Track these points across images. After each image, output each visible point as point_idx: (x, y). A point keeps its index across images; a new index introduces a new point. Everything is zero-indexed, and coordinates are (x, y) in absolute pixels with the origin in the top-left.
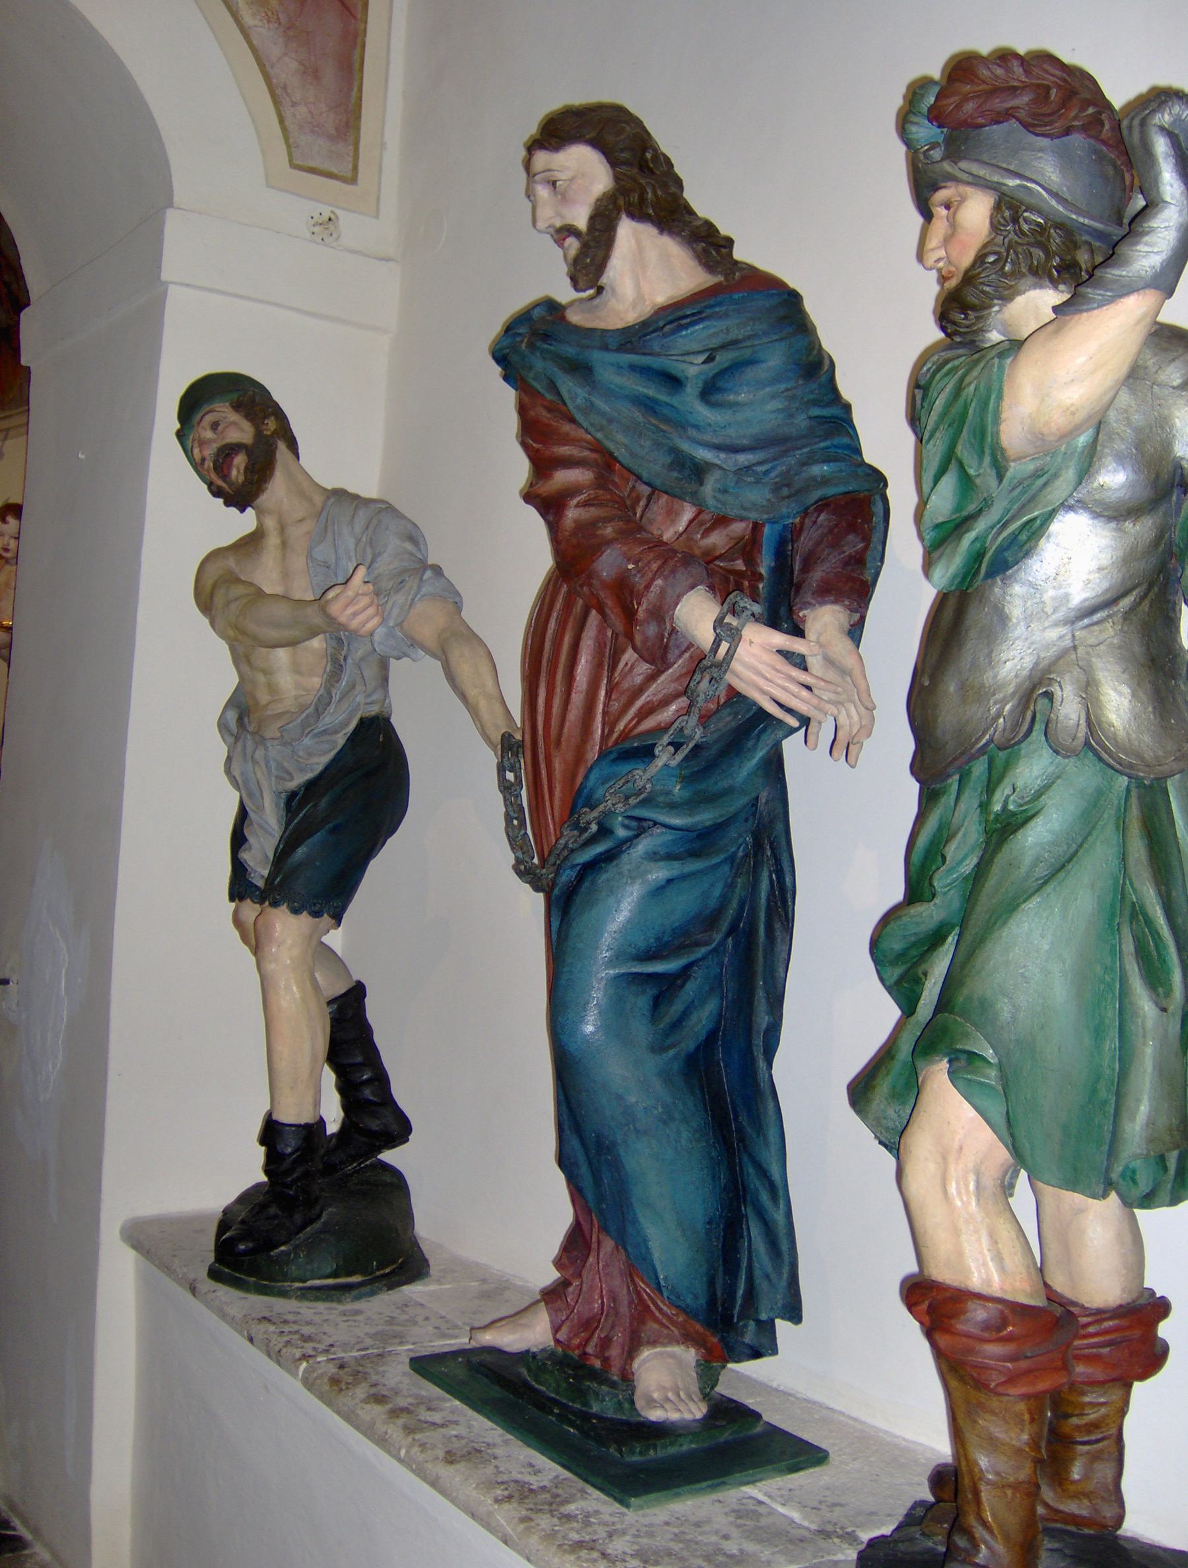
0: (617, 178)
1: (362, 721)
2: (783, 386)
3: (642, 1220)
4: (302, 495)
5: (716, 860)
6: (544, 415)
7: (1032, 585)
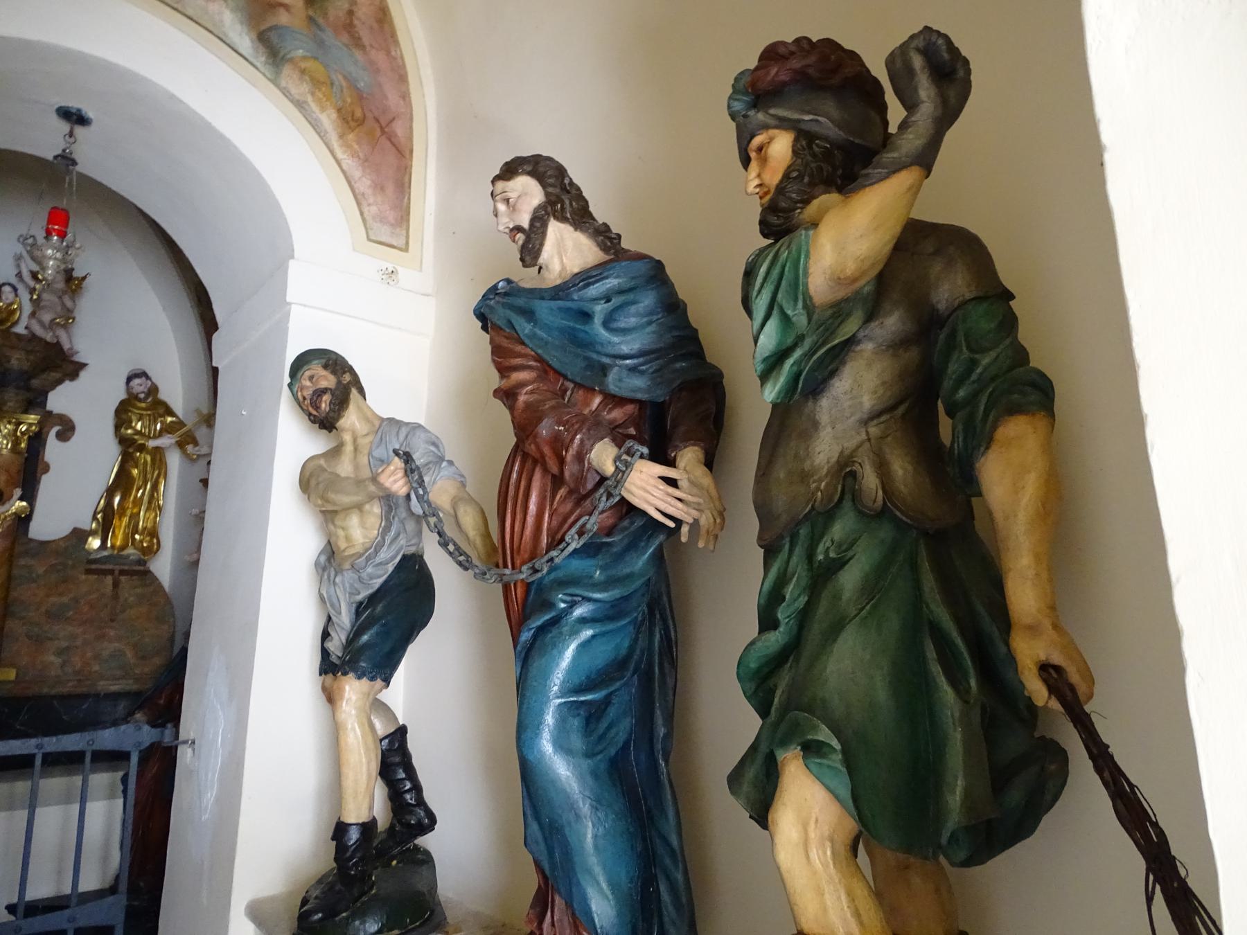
0: (547, 194)
1: (404, 557)
2: (655, 318)
3: (583, 883)
4: (367, 420)
5: (623, 622)
6: (505, 343)
7: (835, 398)
